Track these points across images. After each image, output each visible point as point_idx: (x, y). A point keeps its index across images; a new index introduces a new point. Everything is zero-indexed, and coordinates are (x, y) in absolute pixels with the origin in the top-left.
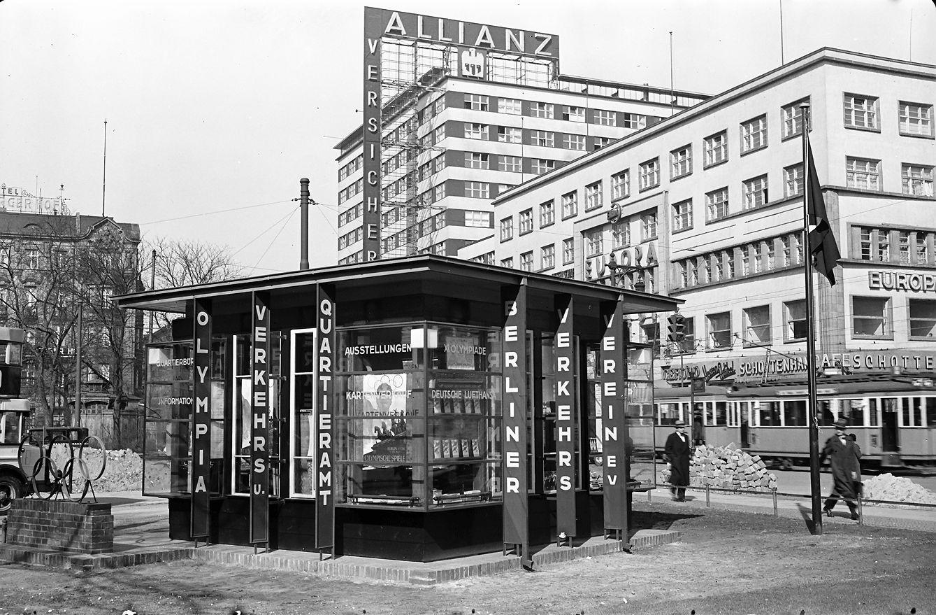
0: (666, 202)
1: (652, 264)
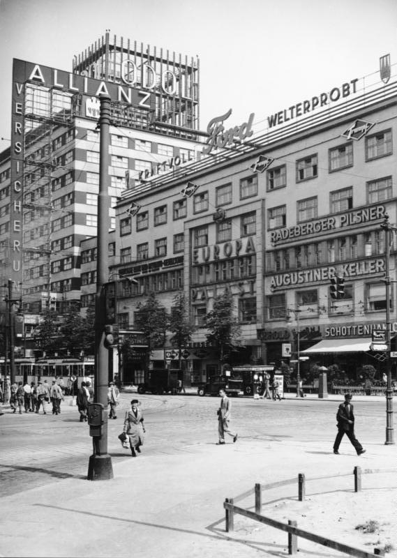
0: (263, 208)
1: (251, 252)
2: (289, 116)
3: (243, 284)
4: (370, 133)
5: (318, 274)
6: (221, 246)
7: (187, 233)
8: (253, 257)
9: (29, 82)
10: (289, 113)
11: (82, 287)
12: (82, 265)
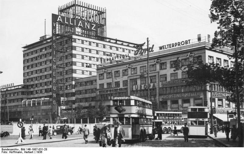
0: (159, 75)
2: (167, 47)
3: (151, 97)
4: (195, 56)
5: (178, 96)
6: (143, 86)
7: (129, 80)
8: (155, 89)
9: (57, 22)
10: (167, 47)
11: (76, 96)
12: (75, 88)
